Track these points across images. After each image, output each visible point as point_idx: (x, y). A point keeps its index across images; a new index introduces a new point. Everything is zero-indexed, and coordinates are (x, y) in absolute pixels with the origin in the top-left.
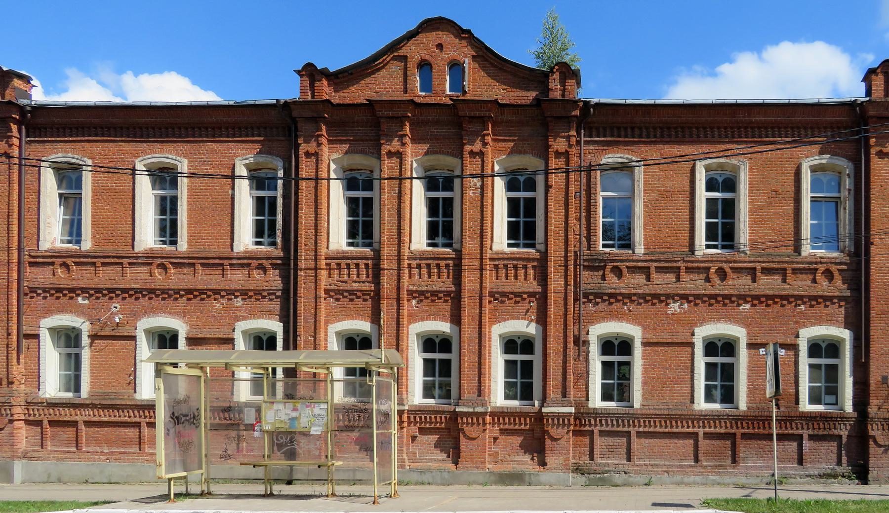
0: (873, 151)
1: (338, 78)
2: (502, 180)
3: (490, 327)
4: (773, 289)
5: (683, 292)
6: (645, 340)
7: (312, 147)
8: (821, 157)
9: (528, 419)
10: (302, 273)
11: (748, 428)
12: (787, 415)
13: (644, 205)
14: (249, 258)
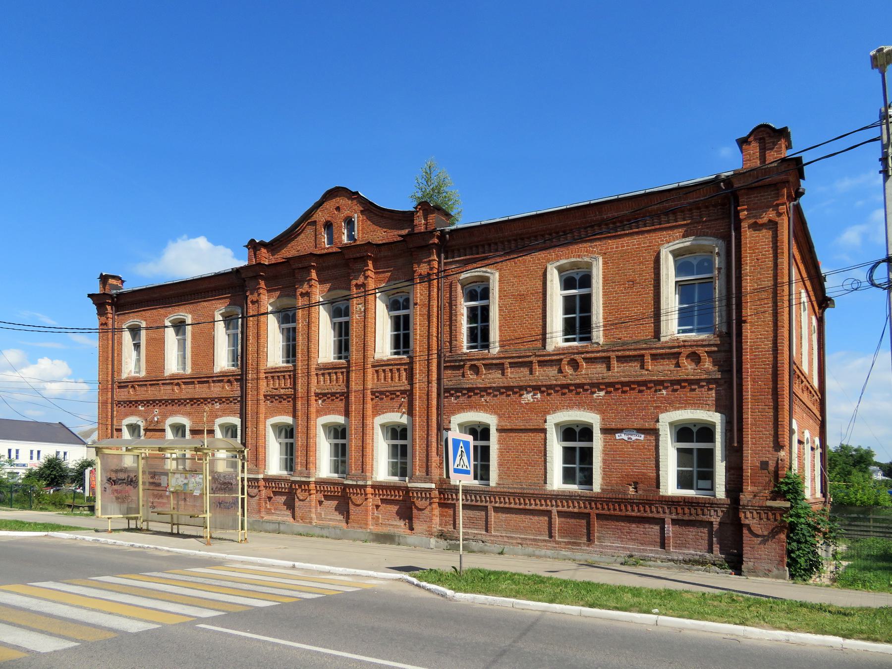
0: (745, 225)
1: (273, 245)
2: (274, 316)
3: (373, 419)
4: (629, 376)
5: (535, 384)
6: (500, 427)
7: (254, 297)
8: (684, 240)
9: (401, 492)
10: (250, 385)
11: (603, 509)
12: (645, 498)
13: (500, 310)
14: (223, 376)
